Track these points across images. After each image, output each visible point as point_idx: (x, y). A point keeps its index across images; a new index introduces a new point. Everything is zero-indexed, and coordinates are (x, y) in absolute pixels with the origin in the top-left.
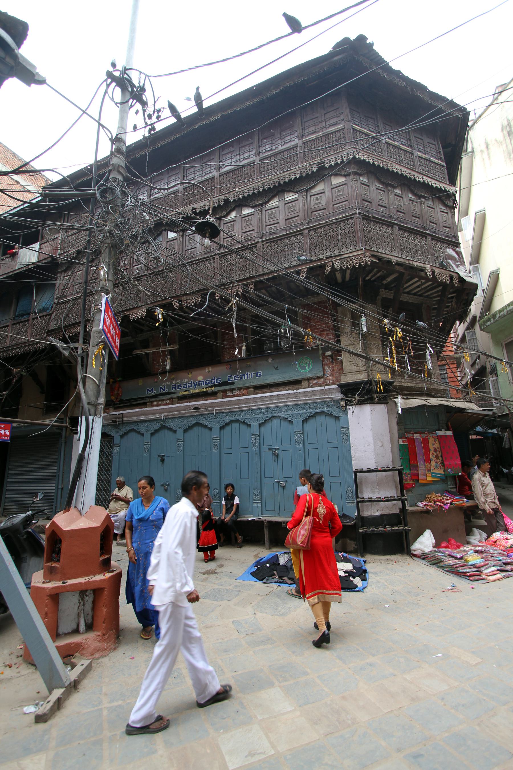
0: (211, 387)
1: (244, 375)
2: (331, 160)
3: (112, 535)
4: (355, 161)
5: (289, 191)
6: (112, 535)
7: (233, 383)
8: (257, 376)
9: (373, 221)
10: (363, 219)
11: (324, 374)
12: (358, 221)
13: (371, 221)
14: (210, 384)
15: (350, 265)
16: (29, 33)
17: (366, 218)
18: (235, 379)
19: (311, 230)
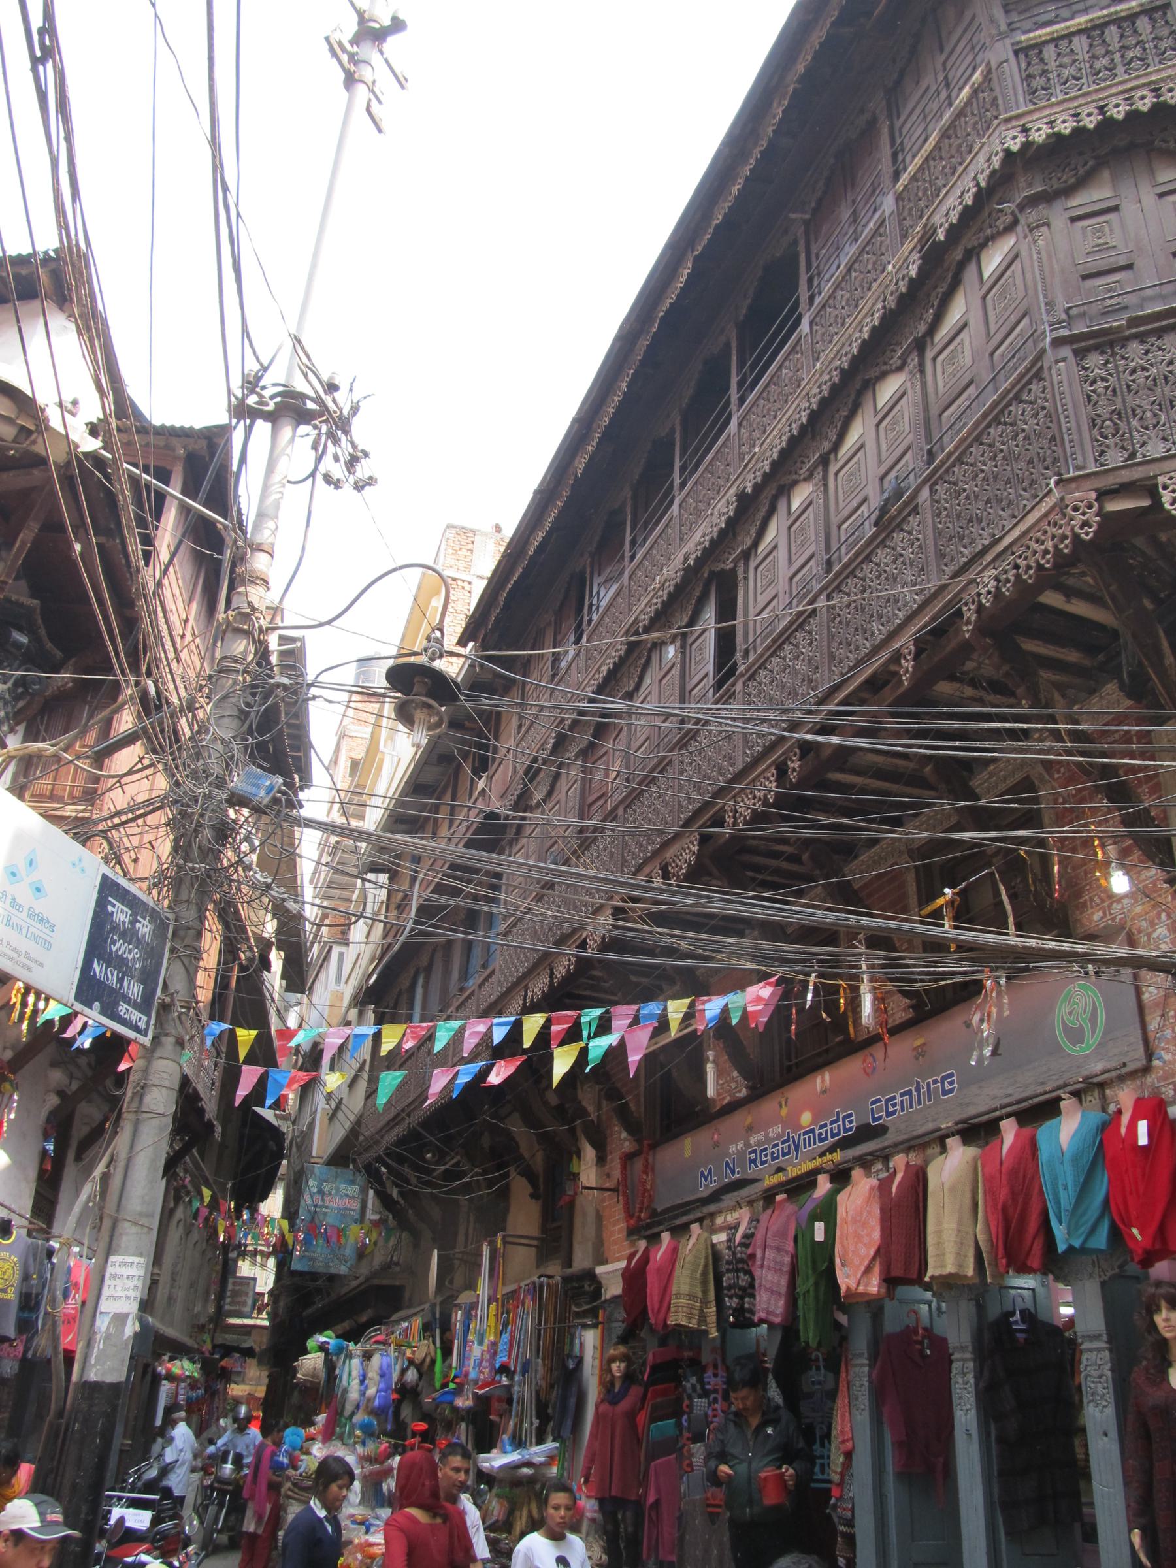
0: (832, 1149)
1: (909, 1093)
2: (947, 211)
3: (97, 1531)
4: (1015, 163)
5: (883, 375)
6: (97, 1531)
7: (882, 1130)
8: (945, 1093)
9: (1135, 336)
10: (1080, 354)
11: (1150, 1055)
12: (1063, 370)
13: (1124, 341)
14: (831, 1140)
15: (1029, 567)
16: (187, 426)
17: (1083, 345)
18: (889, 1114)
19: (936, 483)
